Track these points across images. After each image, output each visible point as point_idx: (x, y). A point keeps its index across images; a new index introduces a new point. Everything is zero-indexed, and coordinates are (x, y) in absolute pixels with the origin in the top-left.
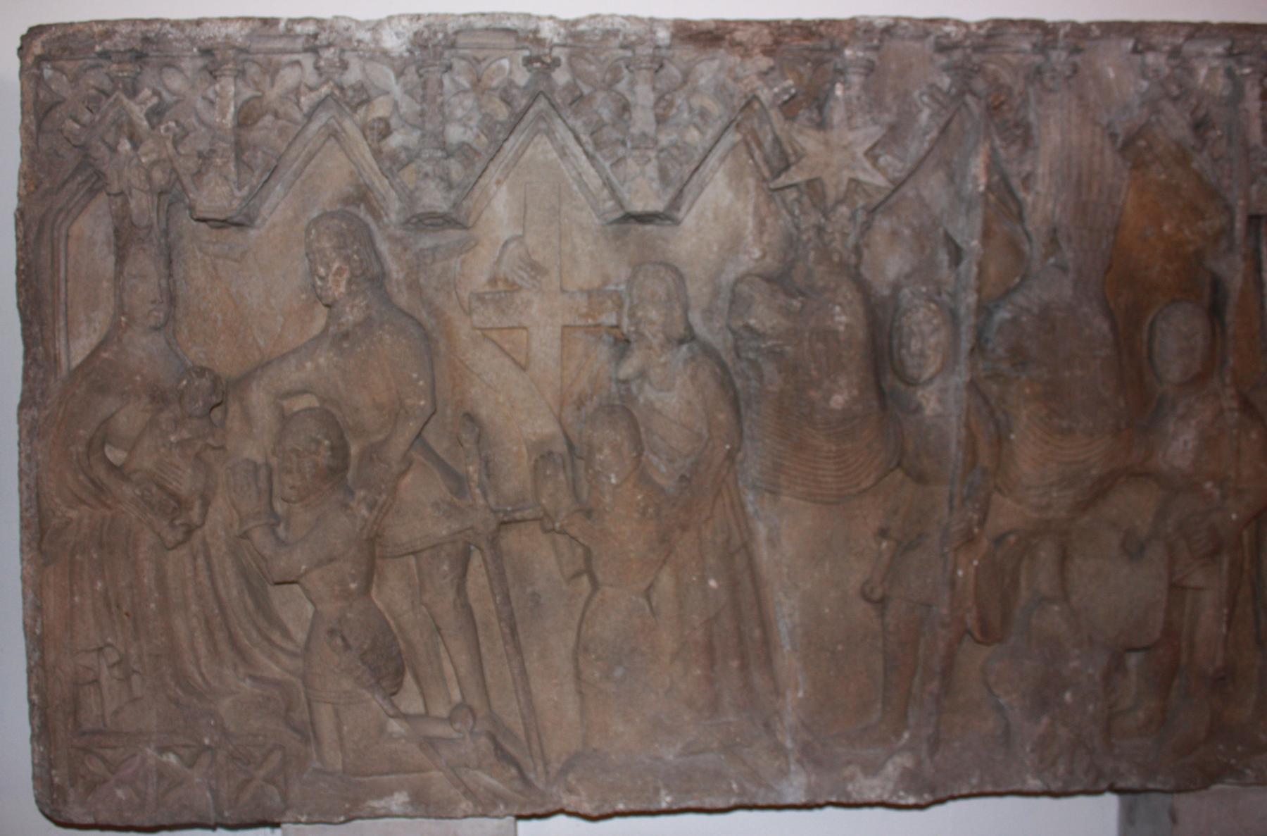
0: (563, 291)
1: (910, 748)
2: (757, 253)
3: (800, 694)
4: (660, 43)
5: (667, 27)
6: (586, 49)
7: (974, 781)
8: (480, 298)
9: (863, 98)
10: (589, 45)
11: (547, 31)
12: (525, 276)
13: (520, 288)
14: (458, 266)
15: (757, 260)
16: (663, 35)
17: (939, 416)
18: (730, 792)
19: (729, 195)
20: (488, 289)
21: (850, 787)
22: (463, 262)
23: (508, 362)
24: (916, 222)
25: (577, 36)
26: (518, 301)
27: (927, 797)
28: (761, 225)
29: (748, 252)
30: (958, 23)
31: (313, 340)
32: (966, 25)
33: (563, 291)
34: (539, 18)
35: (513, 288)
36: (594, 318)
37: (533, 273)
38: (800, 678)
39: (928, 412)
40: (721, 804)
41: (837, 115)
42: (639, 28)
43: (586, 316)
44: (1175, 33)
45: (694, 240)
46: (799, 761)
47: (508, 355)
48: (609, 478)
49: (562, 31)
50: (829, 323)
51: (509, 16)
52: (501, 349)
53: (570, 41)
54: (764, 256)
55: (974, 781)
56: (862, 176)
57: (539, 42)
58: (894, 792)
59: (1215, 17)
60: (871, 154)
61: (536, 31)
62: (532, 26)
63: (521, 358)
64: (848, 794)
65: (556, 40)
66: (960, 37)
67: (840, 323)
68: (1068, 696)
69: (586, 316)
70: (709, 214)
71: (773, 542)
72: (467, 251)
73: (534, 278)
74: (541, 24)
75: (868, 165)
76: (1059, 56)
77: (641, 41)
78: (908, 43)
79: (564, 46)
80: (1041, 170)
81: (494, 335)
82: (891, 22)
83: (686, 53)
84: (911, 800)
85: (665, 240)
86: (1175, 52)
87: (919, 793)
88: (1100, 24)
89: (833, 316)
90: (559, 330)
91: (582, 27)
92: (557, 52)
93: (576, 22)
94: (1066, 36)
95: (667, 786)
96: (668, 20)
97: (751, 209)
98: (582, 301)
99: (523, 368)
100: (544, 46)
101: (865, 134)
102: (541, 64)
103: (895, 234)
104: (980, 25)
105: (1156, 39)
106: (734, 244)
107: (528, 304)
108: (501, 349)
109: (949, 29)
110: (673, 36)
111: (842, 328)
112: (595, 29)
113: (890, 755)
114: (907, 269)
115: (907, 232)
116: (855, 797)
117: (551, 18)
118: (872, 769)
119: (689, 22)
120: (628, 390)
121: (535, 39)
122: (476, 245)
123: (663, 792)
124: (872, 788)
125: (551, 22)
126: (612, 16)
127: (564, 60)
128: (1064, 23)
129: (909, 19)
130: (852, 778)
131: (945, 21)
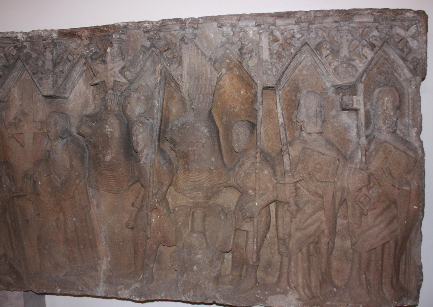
0: (34, 121)
1: (141, 281)
2: (93, 107)
3: (109, 259)
4: (54, 38)
5: (56, 33)
6: (34, 42)
7: (163, 295)
8: (10, 124)
9: (118, 52)
10: (35, 40)
11: (20, 36)
12: (22, 117)
13: (22, 121)
14: (5, 114)
15: (93, 110)
16: (55, 35)
17: (144, 163)
18: (78, 290)
19: (85, 87)
20: (13, 121)
21: (119, 293)
22: (6, 113)
23: (18, 145)
24: (146, 94)
25: (31, 38)
26: (21, 125)
27: (143, 299)
28: (95, 98)
29: (91, 107)
30: (149, 22)
31: (405, 140)
32: (152, 22)
33: (34, 121)
34: (17, 33)
35: (20, 121)
36: (43, 130)
37: (24, 116)
38: (109, 254)
39: (142, 162)
40: (76, 293)
41: (108, 58)
42: (46, 33)
43: (41, 129)
44: (232, 19)
45: (73, 103)
46: (105, 282)
47: (19, 142)
48: (39, 183)
49: (25, 36)
50: (105, 131)
51: (7, 33)
52: (17, 140)
53: (29, 39)
54: (95, 108)
55: (163, 295)
56: (118, 80)
57: (18, 41)
58: (131, 296)
59: (248, 12)
60: (122, 71)
61: (16, 37)
62: (15, 36)
63: (22, 143)
64: (117, 294)
65: (23, 40)
66: (150, 27)
67: (108, 131)
68: (195, 268)
69: (41, 129)
70: (78, 94)
71: (98, 206)
72: (7, 109)
73: (25, 117)
74: (18, 35)
75: (119, 75)
76: (189, 31)
77: (47, 38)
78: (135, 31)
79: (27, 41)
80: (185, 73)
81: (15, 136)
82: (126, 24)
83: (65, 40)
84: (137, 299)
85: (65, 104)
86: (233, 26)
87: (140, 297)
88: (202, 18)
89: (106, 128)
90: (33, 134)
91: (31, 35)
92: (25, 44)
93: (29, 33)
94: (189, 23)
95: (58, 286)
96: (56, 30)
97: (91, 92)
98: (39, 125)
99: (23, 146)
100: (19, 42)
101: (118, 65)
102: (20, 48)
103: (139, 98)
104: (157, 22)
105: (224, 22)
106: (86, 104)
107: (23, 126)
108: (17, 140)
109: (146, 25)
110: (59, 35)
111: (109, 133)
112: (34, 35)
113: (135, 283)
114: (143, 111)
115: (142, 98)
116: (120, 296)
117: (21, 32)
118: (127, 287)
119: (63, 30)
120: (50, 154)
121: (16, 39)
122: (9, 107)
123: (57, 288)
124: (126, 293)
125: (21, 34)
126: (38, 30)
127: (28, 46)
128: (189, 19)
129: (132, 22)
130: (121, 289)
131: (145, 22)
